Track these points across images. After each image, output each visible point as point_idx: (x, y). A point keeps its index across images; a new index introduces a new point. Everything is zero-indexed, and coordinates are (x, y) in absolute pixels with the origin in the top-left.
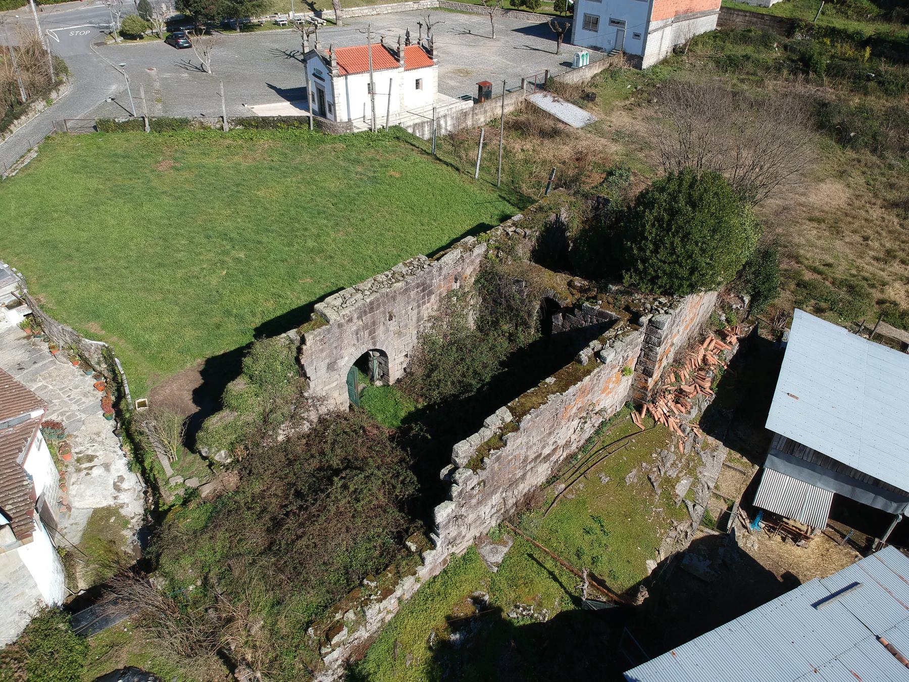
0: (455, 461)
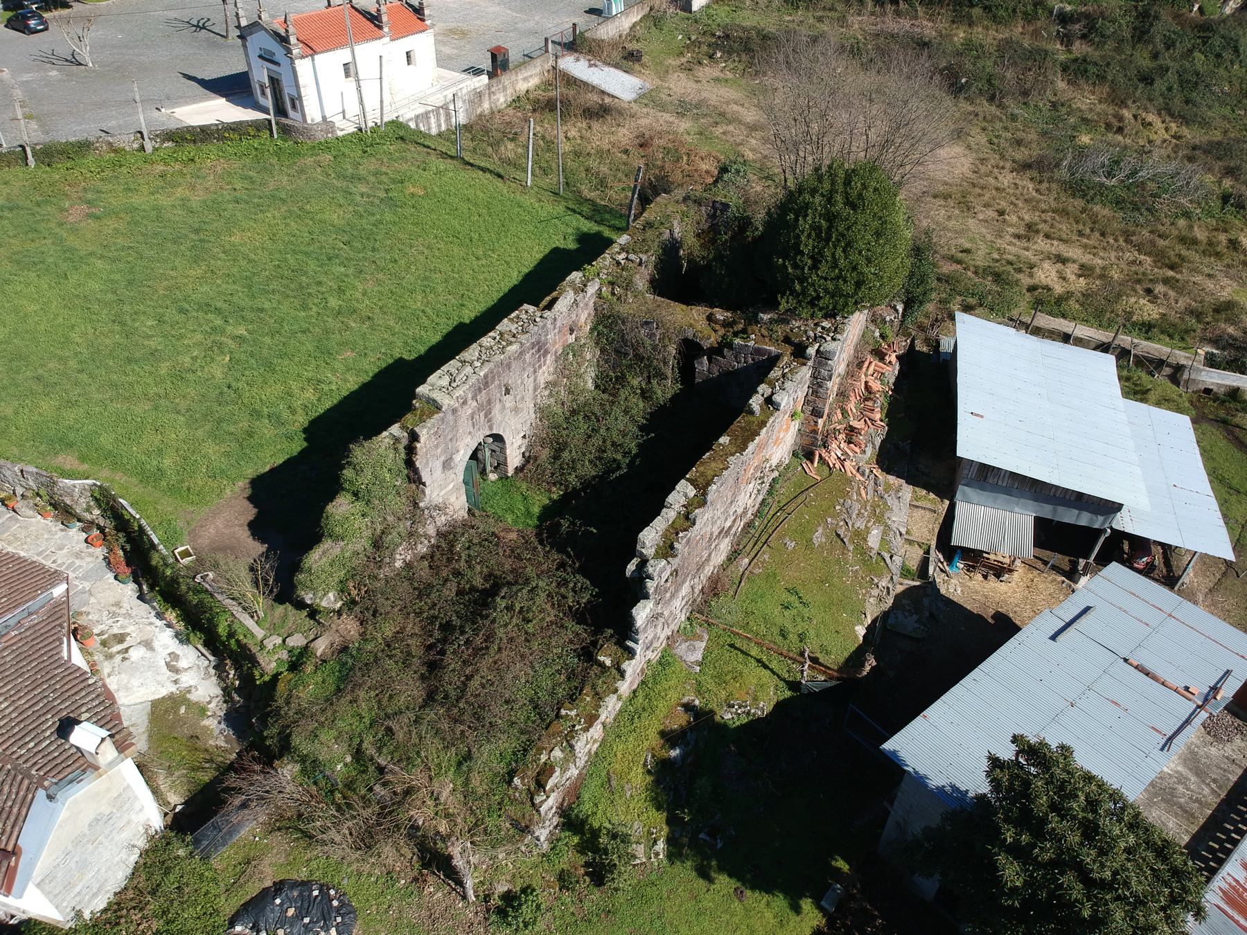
0: (641, 553)
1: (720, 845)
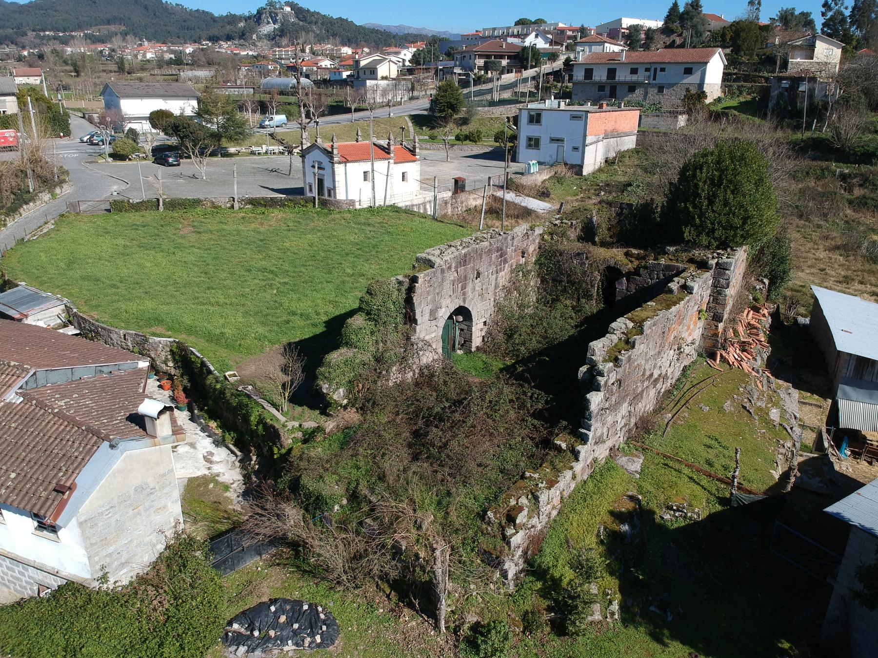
1: (670, 618)
